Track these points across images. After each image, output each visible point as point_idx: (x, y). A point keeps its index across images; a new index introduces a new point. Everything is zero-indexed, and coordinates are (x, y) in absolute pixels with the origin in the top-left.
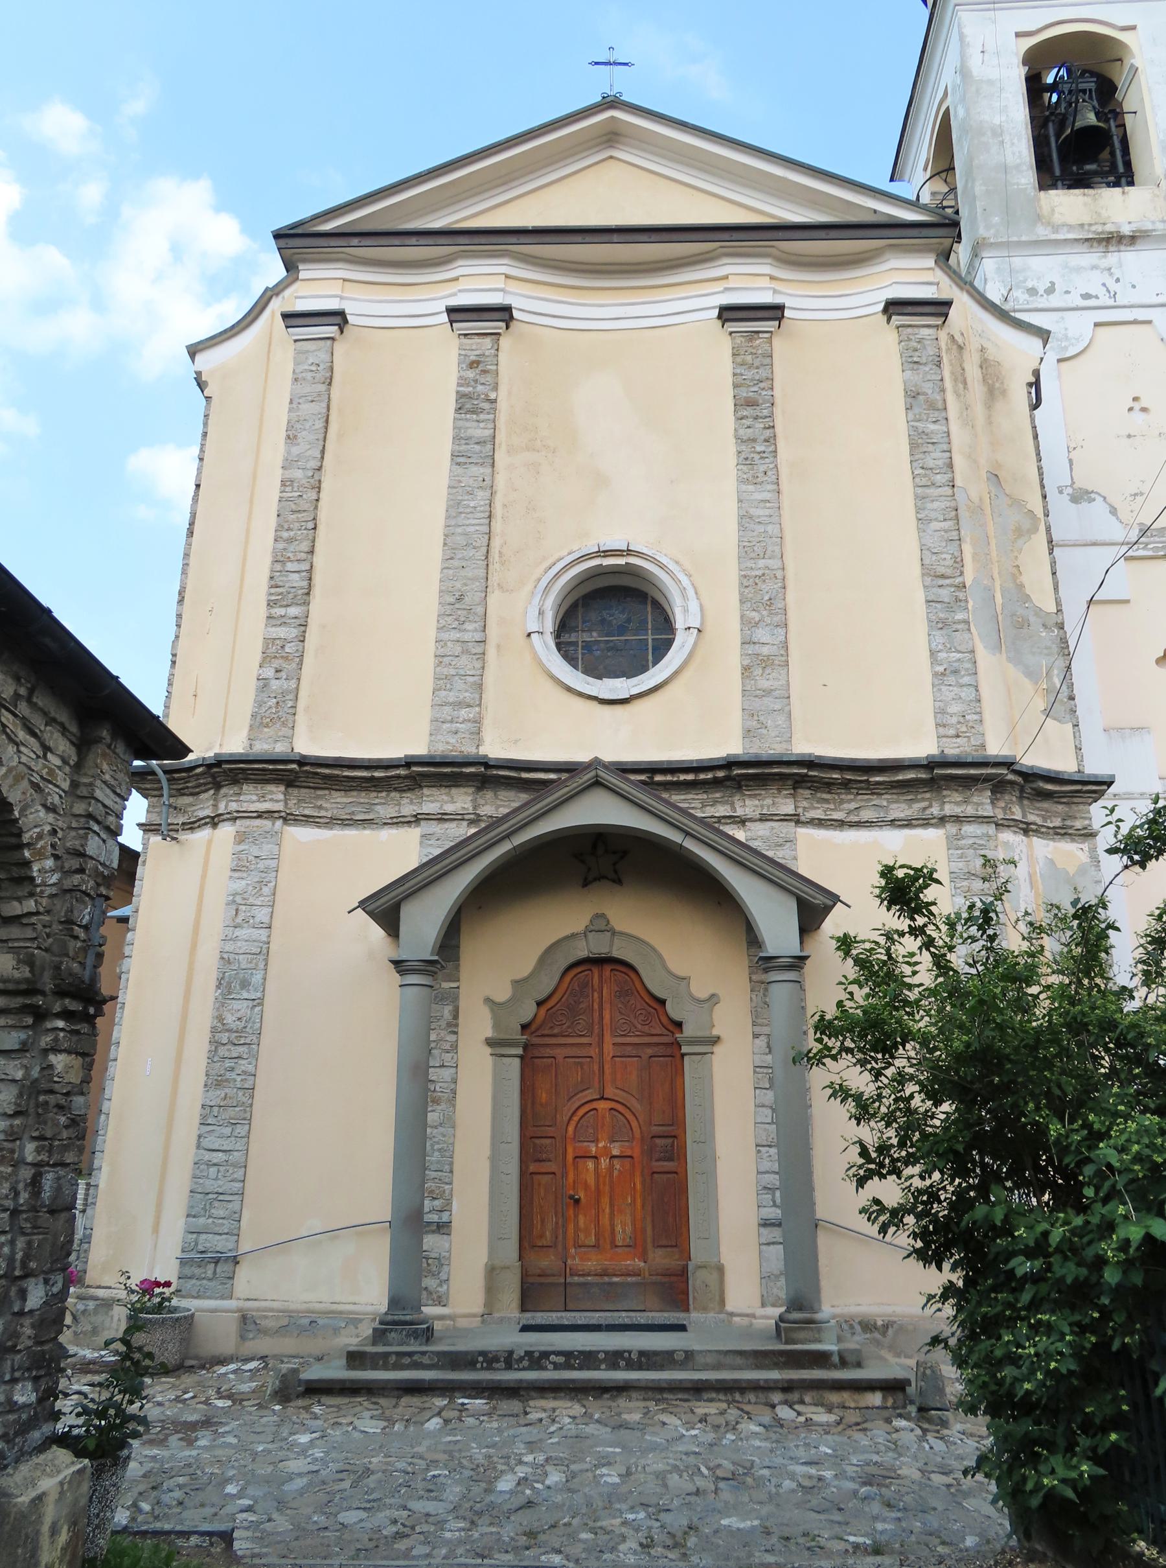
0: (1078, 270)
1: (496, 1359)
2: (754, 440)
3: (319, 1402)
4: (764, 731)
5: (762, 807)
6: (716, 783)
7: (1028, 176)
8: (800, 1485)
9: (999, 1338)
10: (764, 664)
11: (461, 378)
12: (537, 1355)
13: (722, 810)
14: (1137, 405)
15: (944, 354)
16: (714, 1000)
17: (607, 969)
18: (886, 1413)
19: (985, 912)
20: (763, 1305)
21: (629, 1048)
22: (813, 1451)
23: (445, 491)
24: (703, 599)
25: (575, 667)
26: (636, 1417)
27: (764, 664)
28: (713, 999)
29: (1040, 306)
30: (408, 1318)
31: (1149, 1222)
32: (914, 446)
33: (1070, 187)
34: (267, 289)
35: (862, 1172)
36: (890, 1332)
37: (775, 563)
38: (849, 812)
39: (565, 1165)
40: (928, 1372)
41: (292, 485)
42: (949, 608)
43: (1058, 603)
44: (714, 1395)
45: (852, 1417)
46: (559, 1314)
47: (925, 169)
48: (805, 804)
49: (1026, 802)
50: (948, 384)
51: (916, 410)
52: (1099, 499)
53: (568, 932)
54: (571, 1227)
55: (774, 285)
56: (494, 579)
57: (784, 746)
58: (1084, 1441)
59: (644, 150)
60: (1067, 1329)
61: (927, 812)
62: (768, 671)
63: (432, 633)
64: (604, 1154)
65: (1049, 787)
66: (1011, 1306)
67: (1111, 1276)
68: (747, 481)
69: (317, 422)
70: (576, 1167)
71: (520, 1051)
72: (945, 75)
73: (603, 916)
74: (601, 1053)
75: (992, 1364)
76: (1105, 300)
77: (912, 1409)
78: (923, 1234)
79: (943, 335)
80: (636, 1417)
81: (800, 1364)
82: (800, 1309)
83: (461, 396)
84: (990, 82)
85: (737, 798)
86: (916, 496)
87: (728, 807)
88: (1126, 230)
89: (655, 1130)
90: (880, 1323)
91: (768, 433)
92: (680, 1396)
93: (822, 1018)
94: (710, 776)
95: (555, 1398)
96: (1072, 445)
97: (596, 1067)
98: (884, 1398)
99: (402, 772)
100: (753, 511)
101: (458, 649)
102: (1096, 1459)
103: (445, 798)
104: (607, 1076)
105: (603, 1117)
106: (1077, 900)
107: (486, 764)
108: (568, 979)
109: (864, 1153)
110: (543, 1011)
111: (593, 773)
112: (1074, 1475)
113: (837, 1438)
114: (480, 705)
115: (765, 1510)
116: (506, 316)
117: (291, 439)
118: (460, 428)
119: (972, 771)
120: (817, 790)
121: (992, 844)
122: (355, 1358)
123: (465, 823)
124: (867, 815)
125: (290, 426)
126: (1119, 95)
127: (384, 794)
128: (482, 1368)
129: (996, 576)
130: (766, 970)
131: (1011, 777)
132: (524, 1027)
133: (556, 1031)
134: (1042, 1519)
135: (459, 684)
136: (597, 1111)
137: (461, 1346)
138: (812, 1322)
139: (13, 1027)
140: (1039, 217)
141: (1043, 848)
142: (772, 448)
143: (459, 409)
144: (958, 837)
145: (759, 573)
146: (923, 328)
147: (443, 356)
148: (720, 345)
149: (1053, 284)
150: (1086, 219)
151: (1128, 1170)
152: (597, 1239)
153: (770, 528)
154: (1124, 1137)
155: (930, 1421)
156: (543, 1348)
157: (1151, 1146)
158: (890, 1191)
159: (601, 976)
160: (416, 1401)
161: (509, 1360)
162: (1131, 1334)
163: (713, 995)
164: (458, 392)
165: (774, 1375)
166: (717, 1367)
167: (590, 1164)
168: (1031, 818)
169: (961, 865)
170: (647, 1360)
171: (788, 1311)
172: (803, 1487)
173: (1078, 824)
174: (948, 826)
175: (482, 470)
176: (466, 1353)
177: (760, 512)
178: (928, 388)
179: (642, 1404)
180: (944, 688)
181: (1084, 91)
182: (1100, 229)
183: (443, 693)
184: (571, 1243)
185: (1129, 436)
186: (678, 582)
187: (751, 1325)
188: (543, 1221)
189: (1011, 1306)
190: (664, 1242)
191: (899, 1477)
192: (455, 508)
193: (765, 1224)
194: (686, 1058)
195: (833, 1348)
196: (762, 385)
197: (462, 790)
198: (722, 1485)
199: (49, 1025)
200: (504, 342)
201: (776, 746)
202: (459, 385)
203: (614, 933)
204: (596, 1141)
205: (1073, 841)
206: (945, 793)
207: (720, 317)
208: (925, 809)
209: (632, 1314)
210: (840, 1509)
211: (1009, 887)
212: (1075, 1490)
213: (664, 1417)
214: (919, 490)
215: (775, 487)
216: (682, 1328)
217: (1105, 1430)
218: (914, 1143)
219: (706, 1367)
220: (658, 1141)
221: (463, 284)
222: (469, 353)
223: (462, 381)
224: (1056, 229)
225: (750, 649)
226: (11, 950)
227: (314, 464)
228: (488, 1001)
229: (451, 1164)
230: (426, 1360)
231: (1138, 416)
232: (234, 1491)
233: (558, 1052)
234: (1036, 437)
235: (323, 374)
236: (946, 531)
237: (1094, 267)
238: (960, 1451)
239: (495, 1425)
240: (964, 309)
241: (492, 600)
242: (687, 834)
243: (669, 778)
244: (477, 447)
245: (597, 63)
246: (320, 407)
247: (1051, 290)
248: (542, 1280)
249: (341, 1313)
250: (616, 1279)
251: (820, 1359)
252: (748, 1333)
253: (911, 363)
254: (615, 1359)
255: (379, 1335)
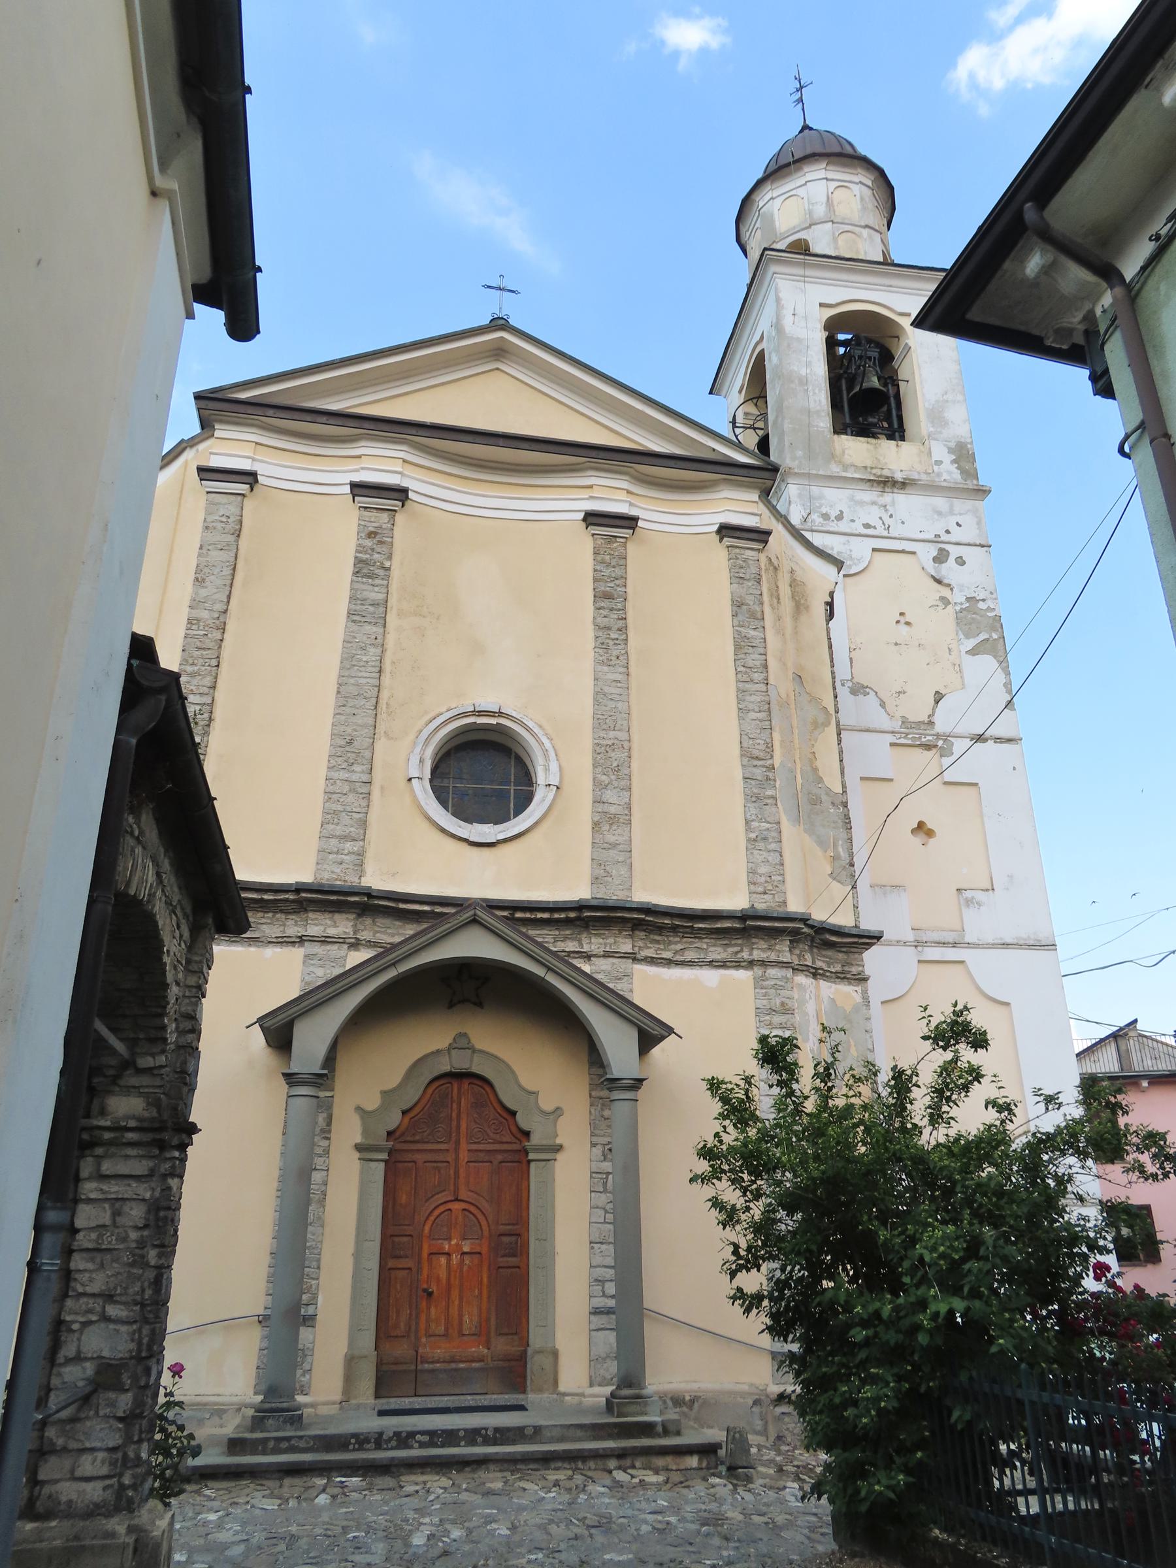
0: (861, 503)
1: (367, 1440)
2: (609, 628)
3: (206, 1486)
4: (610, 879)
5: (605, 944)
6: (568, 922)
7: (824, 421)
8: (654, 1528)
9: (835, 1390)
10: (610, 821)
11: (360, 545)
12: (404, 1435)
13: (571, 946)
14: (903, 619)
15: (763, 573)
16: (559, 1112)
17: (466, 1082)
18: (702, 1473)
19: (827, 1069)
20: (591, 1385)
21: (482, 1155)
22: (653, 1504)
23: (340, 645)
24: (561, 763)
25: (446, 808)
26: (499, 1485)
27: (610, 821)
28: (558, 1112)
29: (832, 529)
30: (285, 1405)
31: (951, 1300)
32: (737, 648)
33: (857, 435)
34: (182, 441)
35: (734, 1267)
36: (696, 1405)
37: (622, 735)
38: (676, 953)
39: (419, 1262)
40: (737, 1435)
41: (198, 624)
42: (761, 785)
43: (844, 786)
44: (560, 1464)
45: (676, 1477)
46: (411, 1399)
47: (740, 392)
48: (640, 944)
49: (815, 950)
50: (766, 598)
51: (740, 617)
52: (872, 693)
53: (433, 1048)
54: (423, 1317)
55: (630, 498)
56: (381, 728)
57: (626, 893)
58: (898, 1460)
59: (523, 366)
60: (890, 1379)
61: (739, 956)
62: (614, 827)
63: (323, 772)
64: (455, 1252)
65: (834, 939)
66: (843, 1365)
67: (923, 1339)
68: (602, 663)
69: (225, 569)
70: (430, 1261)
71: (385, 1156)
72: (762, 324)
73: (465, 1035)
74: (457, 1159)
75: (835, 1410)
76: (881, 531)
77: (723, 1469)
78: (773, 1316)
79: (763, 557)
80: (499, 1485)
81: (630, 1433)
82: (630, 1385)
83: (358, 561)
84: (799, 340)
85: (585, 935)
86: (738, 690)
87: (576, 943)
88: (899, 476)
89: (503, 1228)
90: (687, 1398)
91: (621, 623)
92: (531, 1466)
93: (705, 1146)
94: (563, 916)
95: (422, 1473)
96: (853, 647)
97: (452, 1172)
98: (700, 1460)
99: (291, 897)
100: (606, 689)
101: (346, 788)
102: (908, 1471)
103: (329, 922)
104: (462, 1180)
105: (457, 1218)
106: (896, 1066)
107: (369, 894)
108: (430, 1091)
109: (736, 1252)
110: (406, 1120)
111: (472, 913)
112: (894, 1482)
113: (670, 1494)
114: (364, 840)
115: (634, 1547)
116: (402, 496)
117: (199, 581)
118: (357, 590)
119: (777, 924)
120: (651, 932)
121: (789, 985)
122: (235, 1445)
123: (346, 946)
124: (690, 955)
125: (198, 569)
126: (895, 364)
127: (270, 915)
128: (354, 1450)
129: (798, 761)
130: (610, 1090)
131: (806, 930)
132: (389, 1134)
133: (417, 1138)
134: (861, 1525)
135: (345, 819)
136: (453, 1209)
137: (332, 1430)
138: (639, 1397)
139: (143, 1156)
140: (833, 456)
141: (827, 989)
142: (624, 637)
143: (356, 573)
144: (763, 978)
145: (610, 743)
146: (748, 551)
147: (345, 524)
148: (584, 543)
149: (842, 512)
150: (869, 463)
151: (936, 1264)
152: (447, 1329)
153: (620, 705)
154: (933, 1241)
155: (737, 1478)
156: (409, 1429)
157: (951, 1247)
158: (754, 1281)
159: (459, 1089)
160: (297, 1481)
161: (379, 1441)
162: (933, 1379)
163: (558, 1108)
164: (356, 558)
165: (611, 1444)
166: (561, 1440)
167: (443, 1260)
168: (819, 964)
169: (765, 1002)
170: (502, 1435)
171: (619, 1387)
172: (658, 1529)
173: (854, 970)
174: (756, 969)
175: (375, 629)
176: (340, 1436)
177: (612, 690)
178: (750, 600)
179: (499, 1475)
180: (755, 852)
181: (870, 358)
182: (879, 472)
183: (331, 827)
184: (423, 1332)
185: (896, 644)
186: (541, 744)
187: (581, 1403)
188: (398, 1312)
189: (843, 1365)
190: (506, 1330)
191: (727, 1519)
192: (348, 661)
193: (596, 1312)
194: (533, 1165)
195: (658, 1419)
196: (617, 582)
197: (345, 916)
198: (593, 1531)
199: (168, 1155)
200: (399, 518)
201: (618, 893)
202: (357, 551)
203: (474, 1051)
204: (449, 1239)
205: (850, 984)
206: (754, 940)
207: (584, 520)
208: (737, 953)
209: (478, 1397)
210: (691, 1544)
211: (840, 1048)
212: (894, 1492)
213: (523, 1484)
214: (741, 685)
215: (624, 670)
216: (521, 1408)
217: (912, 1451)
218: (767, 1241)
219: (552, 1440)
220: (505, 1239)
221: (365, 462)
222: (368, 524)
223: (361, 549)
224: (845, 468)
225: (600, 807)
226: (141, 1094)
227: (220, 607)
228: (359, 1109)
229: (319, 1260)
230: (302, 1444)
231: (904, 629)
232: (184, 1559)
233: (418, 1157)
234: (830, 647)
235: (232, 526)
236: (761, 721)
237: (874, 503)
238: (765, 1500)
239: (378, 1497)
240: (780, 538)
241: (378, 746)
242: (549, 969)
243: (528, 915)
244: (371, 609)
245: (489, 287)
246: (228, 556)
247: (840, 517)
248: (394, 1368)
249: (205, 1404)
250: (462, 1365)
251: (647, 1429)
252: (580, 1410)
253: (738, 578)
254: (473, 1436)
255: (258, 1422)
